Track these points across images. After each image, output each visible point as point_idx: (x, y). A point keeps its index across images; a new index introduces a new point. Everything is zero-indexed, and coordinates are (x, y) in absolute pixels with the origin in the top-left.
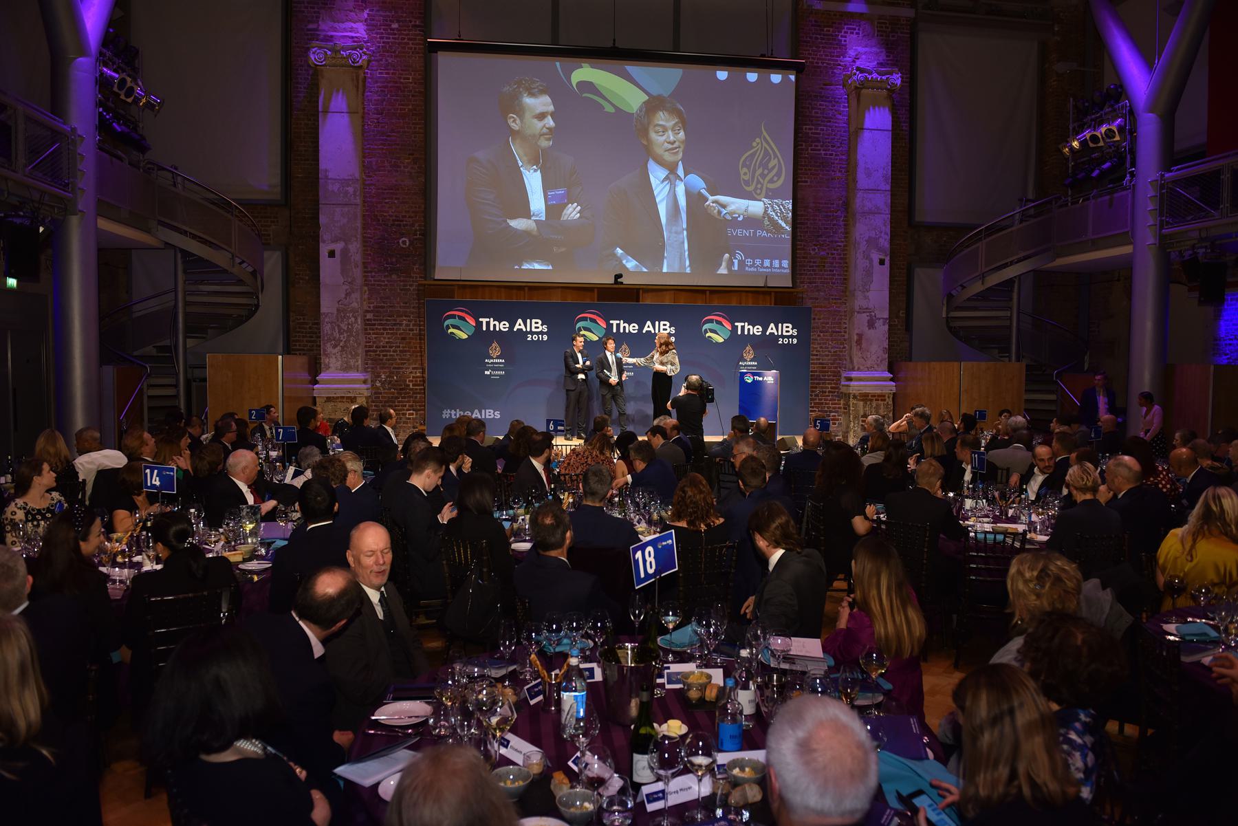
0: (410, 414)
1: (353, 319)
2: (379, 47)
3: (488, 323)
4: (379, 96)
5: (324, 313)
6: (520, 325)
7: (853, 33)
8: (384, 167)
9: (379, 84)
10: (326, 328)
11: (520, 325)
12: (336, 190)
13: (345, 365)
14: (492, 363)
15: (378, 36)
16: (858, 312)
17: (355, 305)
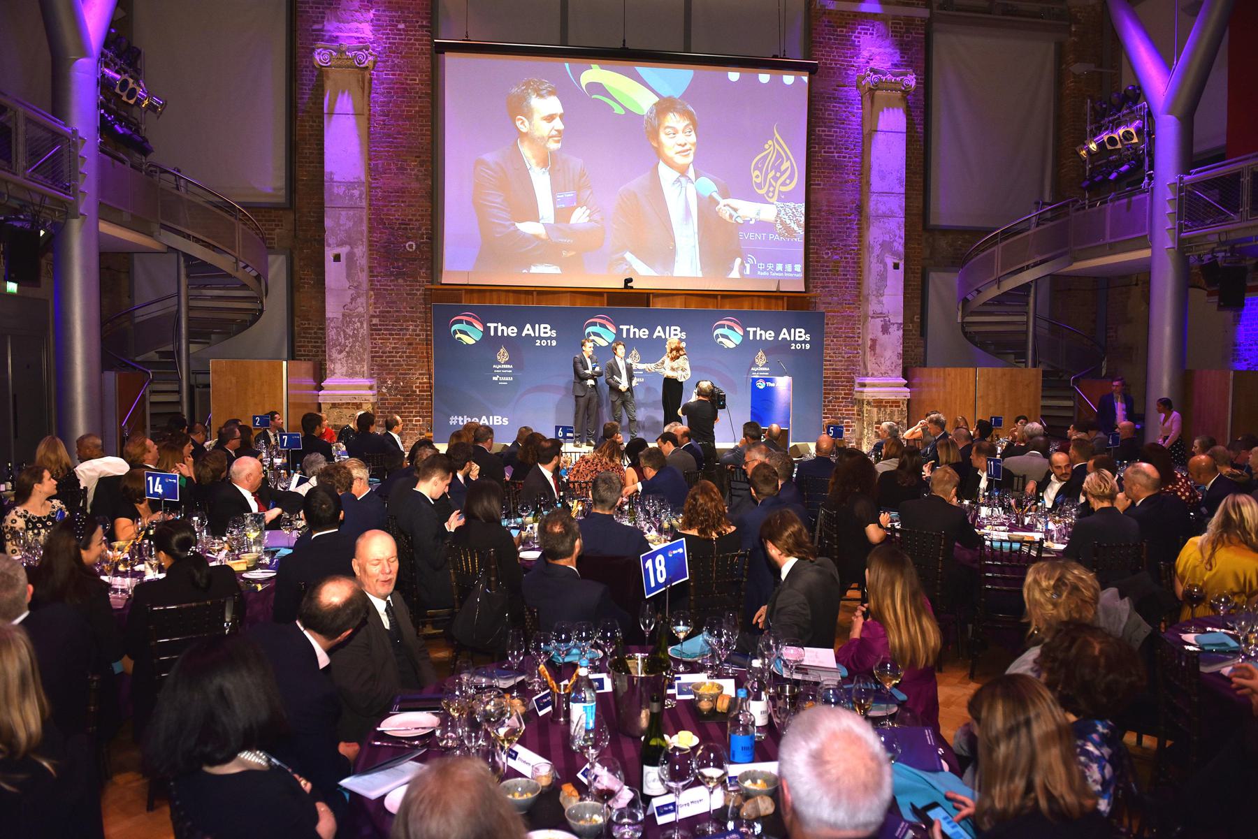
0: (416, 421)
3: (496, 328)
4: (385, 97)
7: (866, 34)
8: (390, 169)
10: (331, 334)
16: (872, 317)
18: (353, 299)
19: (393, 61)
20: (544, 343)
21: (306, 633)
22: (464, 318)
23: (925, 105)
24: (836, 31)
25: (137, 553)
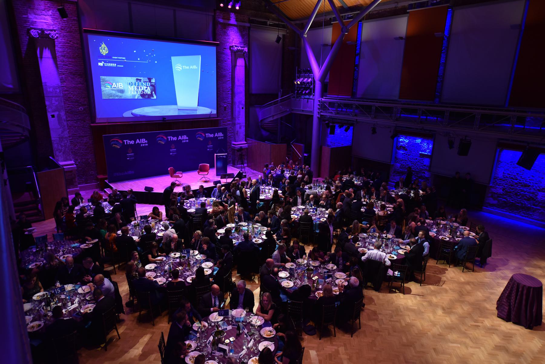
0: (91, 173)
1: (66, 141)
2: (59, 28)
3: (127, 142)
4: (62, 49)
5: (53, 140)
6: (138, 141)
7: (232, 31)
8: (68, 79)
9: (61, 44)
10: (55, 146)
11: (138, 141)
12: (51, 91)
13: (65, 159)
14: (130, 155)
15: (58, 23)
16: (237, 124)
17: (66, 136)
18: (62, 132)
19: (63, 34)
22: (115, 139)
23: (249, 56)
24: (223, 30)
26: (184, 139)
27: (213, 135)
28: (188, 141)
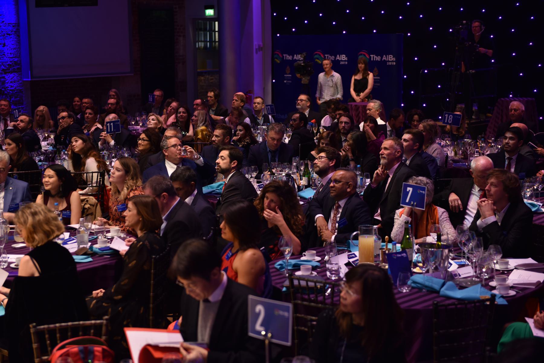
20: (390, 63)
21: (382, 201)
22: (363, 53)
25: (24, 233)
26: (390, 60)
27: (380, 58)
28: (346, 63)
